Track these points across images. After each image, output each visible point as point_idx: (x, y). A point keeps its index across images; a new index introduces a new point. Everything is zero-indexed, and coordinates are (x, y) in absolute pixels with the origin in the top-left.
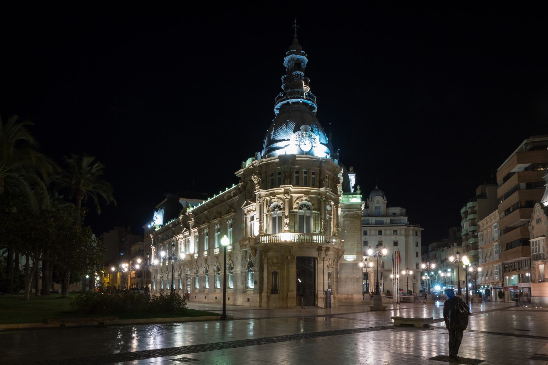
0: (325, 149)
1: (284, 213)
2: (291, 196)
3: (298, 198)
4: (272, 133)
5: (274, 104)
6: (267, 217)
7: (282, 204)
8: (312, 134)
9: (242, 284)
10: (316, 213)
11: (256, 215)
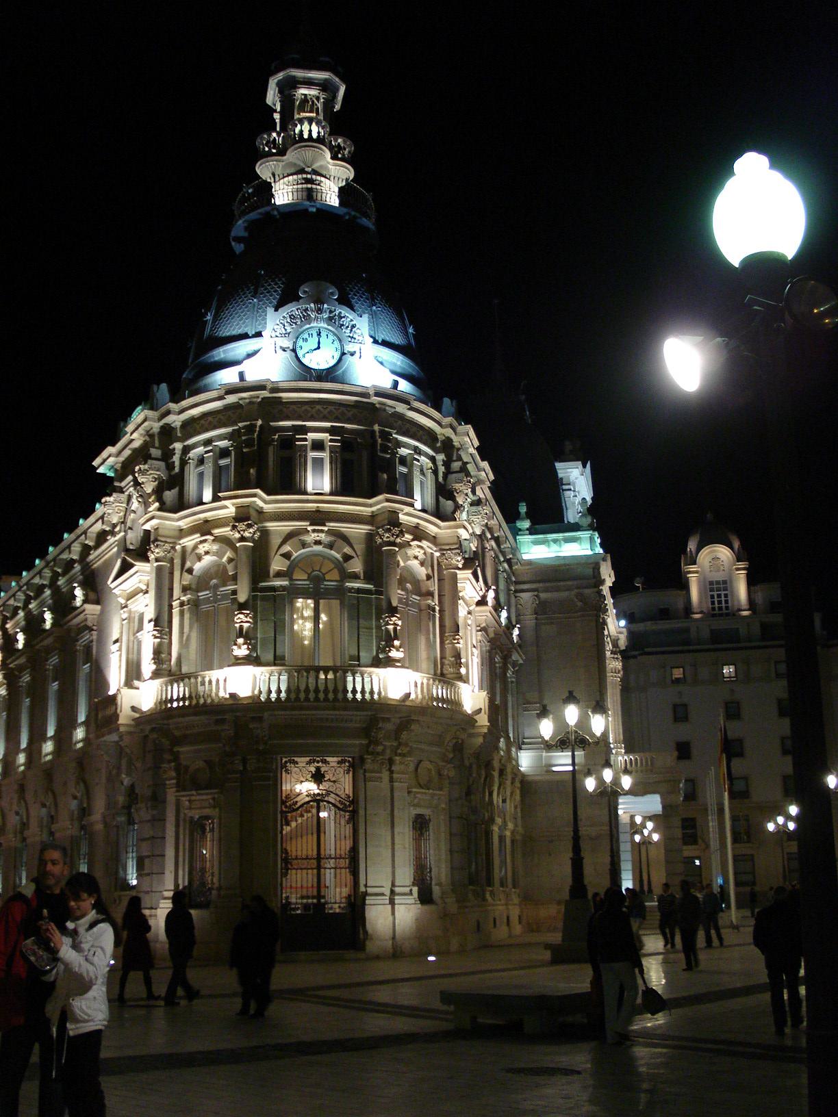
0: (395, 359)
1: (234, 592)
2: (265, 533)
3: (290, 536)
4: (209, 317)
5: (230, 220)
6: (182, 614)
7: (230, 560)
8: (344, 311)
9: (346, 876)
10: (359, 591)
11: (146, 606)
